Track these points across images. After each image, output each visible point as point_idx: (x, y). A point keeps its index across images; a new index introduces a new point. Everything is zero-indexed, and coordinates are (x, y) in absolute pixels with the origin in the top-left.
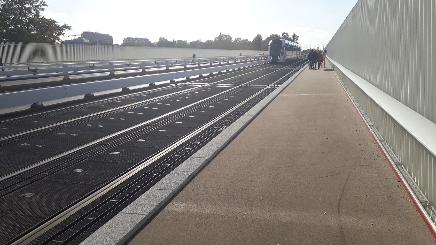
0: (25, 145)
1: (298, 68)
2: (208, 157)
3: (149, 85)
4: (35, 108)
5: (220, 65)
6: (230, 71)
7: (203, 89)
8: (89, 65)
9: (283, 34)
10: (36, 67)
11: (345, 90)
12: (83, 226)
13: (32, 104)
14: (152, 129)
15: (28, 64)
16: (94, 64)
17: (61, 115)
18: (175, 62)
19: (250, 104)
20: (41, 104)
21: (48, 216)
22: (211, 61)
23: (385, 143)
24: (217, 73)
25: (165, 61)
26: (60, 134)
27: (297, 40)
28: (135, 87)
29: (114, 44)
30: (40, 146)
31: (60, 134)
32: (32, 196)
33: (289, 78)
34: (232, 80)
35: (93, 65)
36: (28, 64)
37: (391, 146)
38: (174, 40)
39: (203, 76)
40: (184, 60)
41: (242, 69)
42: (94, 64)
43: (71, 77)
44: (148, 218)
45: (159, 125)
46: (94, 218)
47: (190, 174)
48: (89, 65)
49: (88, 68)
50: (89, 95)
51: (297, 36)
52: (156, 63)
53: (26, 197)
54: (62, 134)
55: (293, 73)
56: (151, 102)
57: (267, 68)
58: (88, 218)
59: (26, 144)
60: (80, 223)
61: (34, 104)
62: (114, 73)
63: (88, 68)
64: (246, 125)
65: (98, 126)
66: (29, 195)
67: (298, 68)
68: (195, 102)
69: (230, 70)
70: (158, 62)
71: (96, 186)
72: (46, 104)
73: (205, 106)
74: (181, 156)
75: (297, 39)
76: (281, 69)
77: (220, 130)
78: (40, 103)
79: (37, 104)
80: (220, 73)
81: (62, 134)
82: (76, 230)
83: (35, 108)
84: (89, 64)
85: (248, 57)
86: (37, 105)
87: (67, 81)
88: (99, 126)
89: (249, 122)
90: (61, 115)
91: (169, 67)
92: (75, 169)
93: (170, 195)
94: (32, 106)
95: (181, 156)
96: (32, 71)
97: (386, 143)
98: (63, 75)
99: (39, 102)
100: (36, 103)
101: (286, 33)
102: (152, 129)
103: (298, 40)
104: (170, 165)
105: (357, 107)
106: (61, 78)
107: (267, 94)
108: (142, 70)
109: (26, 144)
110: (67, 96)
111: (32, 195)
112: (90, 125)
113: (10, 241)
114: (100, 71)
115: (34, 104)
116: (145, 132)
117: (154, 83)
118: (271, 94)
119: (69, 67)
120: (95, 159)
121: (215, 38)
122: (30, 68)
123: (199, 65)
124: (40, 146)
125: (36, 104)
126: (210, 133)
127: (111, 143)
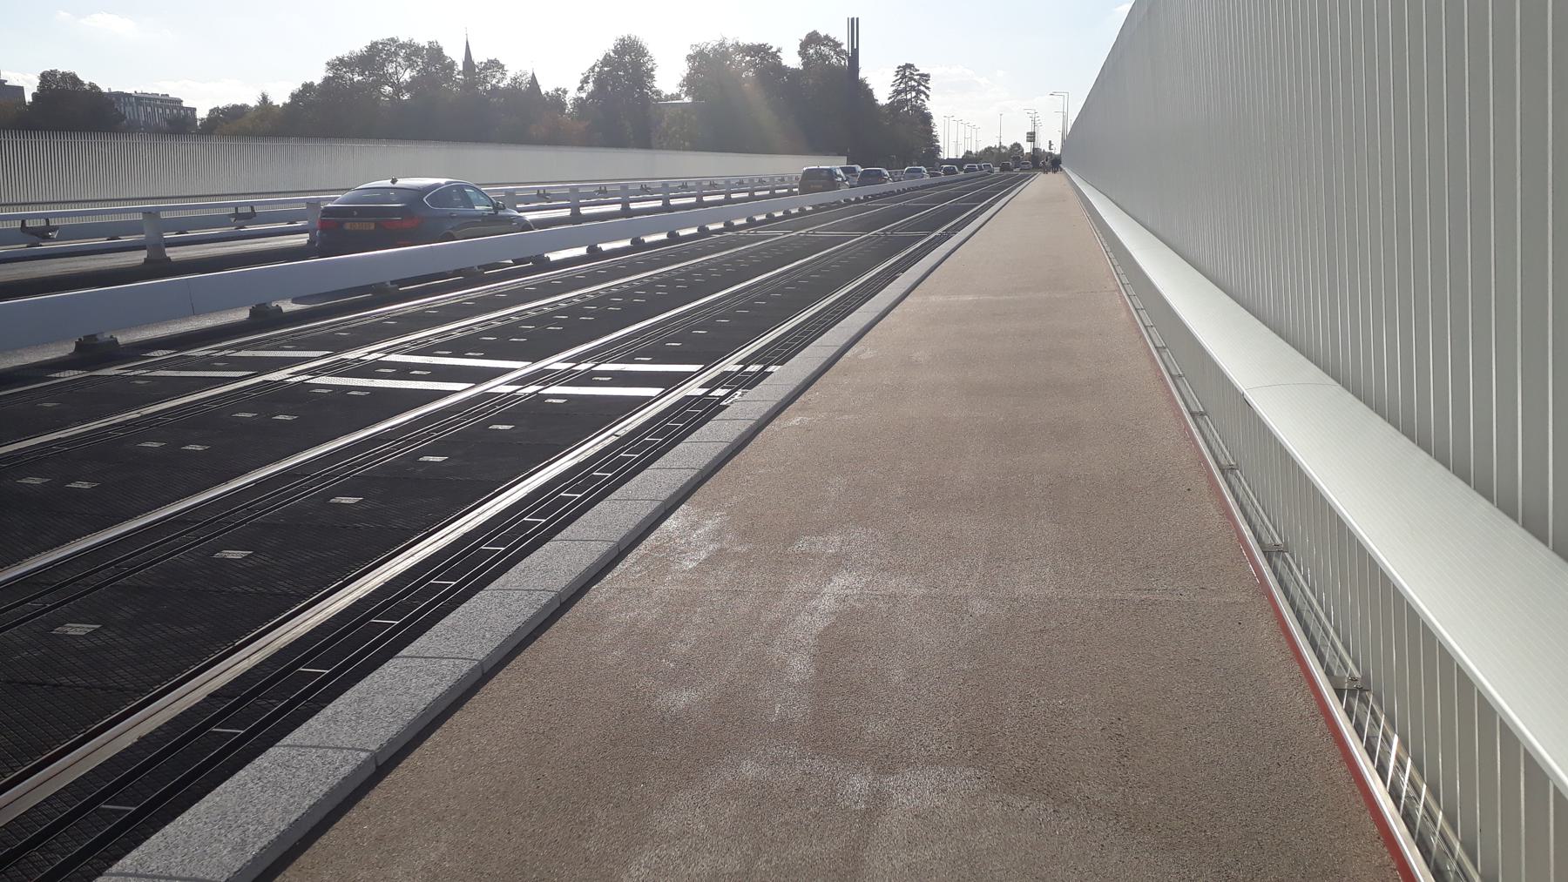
0: (31, 482)
1: (945, 228)
2: (373, 748)
3: (588, 251)
4: (93, 353)
5: (728, 200)
6: (759, 221)
7: (659, 280)
8: (236, 209)
9: (804, 46)
10: (47, 221)
11: (1146, 335)
12: (95, 833)
13: (80, 339)
14: (465, 424)
15: (23, 209)
16: (252, 208)
17: (45, 405)
18: (538, 194)
19: (787, 346)
20: (111, 337)
21: (55, 744)
22: (666, 192)
23: (1285, 560)
24: (663, 236)
25: (305, 204)
26: (149, 445)
27: (923, 97)
28: (182, 325)
29: (846, 158)
30: (85, 485)
31: (149, 445)
32: (89, 631)
33: (883, 288)
34: (752, 254)
35: (249, 210)
36: (23, 209)
37: (1275, 521)
38: (265, 98)
39: (552, 259)
40: (144, 213)
41: (780, 218)
42: (252, 208)
43: (174, 254)
44: (564, 599)
45: (488, 409)
46: (132, 806)
47: (466, 667)
48: (236, 209)
49: (233, 220)
50: (96, 339)
51: (922, 75)
52: (683, 187)
53: (69, 636)
54: (156, 445)
55: (928, 245)
56: (457, 335)
57: (807, 233)
58: (112, 804)
59: (36, 481)
60: (121, 795)
61: (84, 337)
62: (168, 255)
63: (233, 220)
64: (797, 392)
65: (187, 448)
66: (78, 630)
67: (945, 228)
68: (744, 281)
69: (758, 218)
70: (255, 207)
71: (136, 691)
72: (554, 256)
73: (649, 343)
74: (503, 549)
75: (922, 88)
76: (869, 237)
77: (724, 403)
78: (107, 336)
79: (99, 337)
80: (674, 238)
81: (156, 445)
82: (274, 701)
83: (93, 353)
84: (236, 206)
85: (761, 181)
86: (98, 342)
87: (158, 267)
88: (280, 417)
89: (478, 675)
90: (45, 405)
91: (581, 208)
92: (62, 625)
93: (546, 606)
94: (79, 345)
95: (503, 549)
96: (32, 234)
97: (1254, 499)
98: (619, 203)
99: (102, 333)
100: (94, 336)
101: (827, 37)
102: (465, 424)
103: (927, 96)
104: (242, 732)
105: (1156, 347)
106: (139, 257)
107: (1003, 197)
108: (308, 235)
109: (36, 481)
110: (195, 312)
111: (88, 628)
112: (250, 415)
113: (72, 741)
114: (206, 238)
115: (84, 337)
116: (365, 468)
117: (274, 305)
118: (453, 627)
119: (164, 215)
120: (150, 580)
121: (332, 66)
122: (29, 224)
123: (625, 204)
124: (85, 485)
125: (93, 336)
126: (606, 470)
127: (330, 470)
